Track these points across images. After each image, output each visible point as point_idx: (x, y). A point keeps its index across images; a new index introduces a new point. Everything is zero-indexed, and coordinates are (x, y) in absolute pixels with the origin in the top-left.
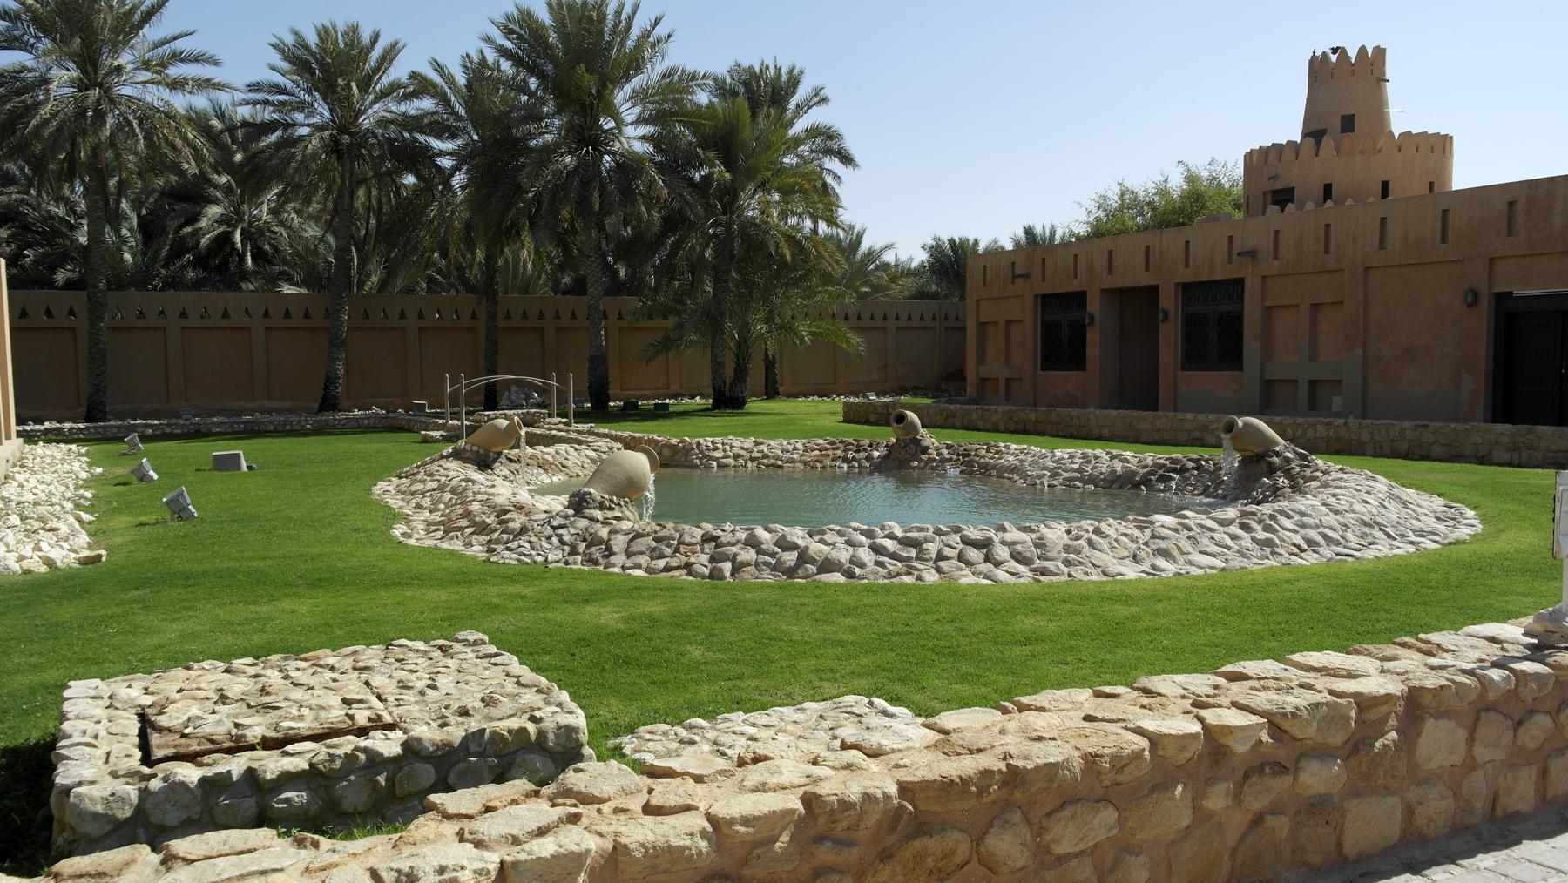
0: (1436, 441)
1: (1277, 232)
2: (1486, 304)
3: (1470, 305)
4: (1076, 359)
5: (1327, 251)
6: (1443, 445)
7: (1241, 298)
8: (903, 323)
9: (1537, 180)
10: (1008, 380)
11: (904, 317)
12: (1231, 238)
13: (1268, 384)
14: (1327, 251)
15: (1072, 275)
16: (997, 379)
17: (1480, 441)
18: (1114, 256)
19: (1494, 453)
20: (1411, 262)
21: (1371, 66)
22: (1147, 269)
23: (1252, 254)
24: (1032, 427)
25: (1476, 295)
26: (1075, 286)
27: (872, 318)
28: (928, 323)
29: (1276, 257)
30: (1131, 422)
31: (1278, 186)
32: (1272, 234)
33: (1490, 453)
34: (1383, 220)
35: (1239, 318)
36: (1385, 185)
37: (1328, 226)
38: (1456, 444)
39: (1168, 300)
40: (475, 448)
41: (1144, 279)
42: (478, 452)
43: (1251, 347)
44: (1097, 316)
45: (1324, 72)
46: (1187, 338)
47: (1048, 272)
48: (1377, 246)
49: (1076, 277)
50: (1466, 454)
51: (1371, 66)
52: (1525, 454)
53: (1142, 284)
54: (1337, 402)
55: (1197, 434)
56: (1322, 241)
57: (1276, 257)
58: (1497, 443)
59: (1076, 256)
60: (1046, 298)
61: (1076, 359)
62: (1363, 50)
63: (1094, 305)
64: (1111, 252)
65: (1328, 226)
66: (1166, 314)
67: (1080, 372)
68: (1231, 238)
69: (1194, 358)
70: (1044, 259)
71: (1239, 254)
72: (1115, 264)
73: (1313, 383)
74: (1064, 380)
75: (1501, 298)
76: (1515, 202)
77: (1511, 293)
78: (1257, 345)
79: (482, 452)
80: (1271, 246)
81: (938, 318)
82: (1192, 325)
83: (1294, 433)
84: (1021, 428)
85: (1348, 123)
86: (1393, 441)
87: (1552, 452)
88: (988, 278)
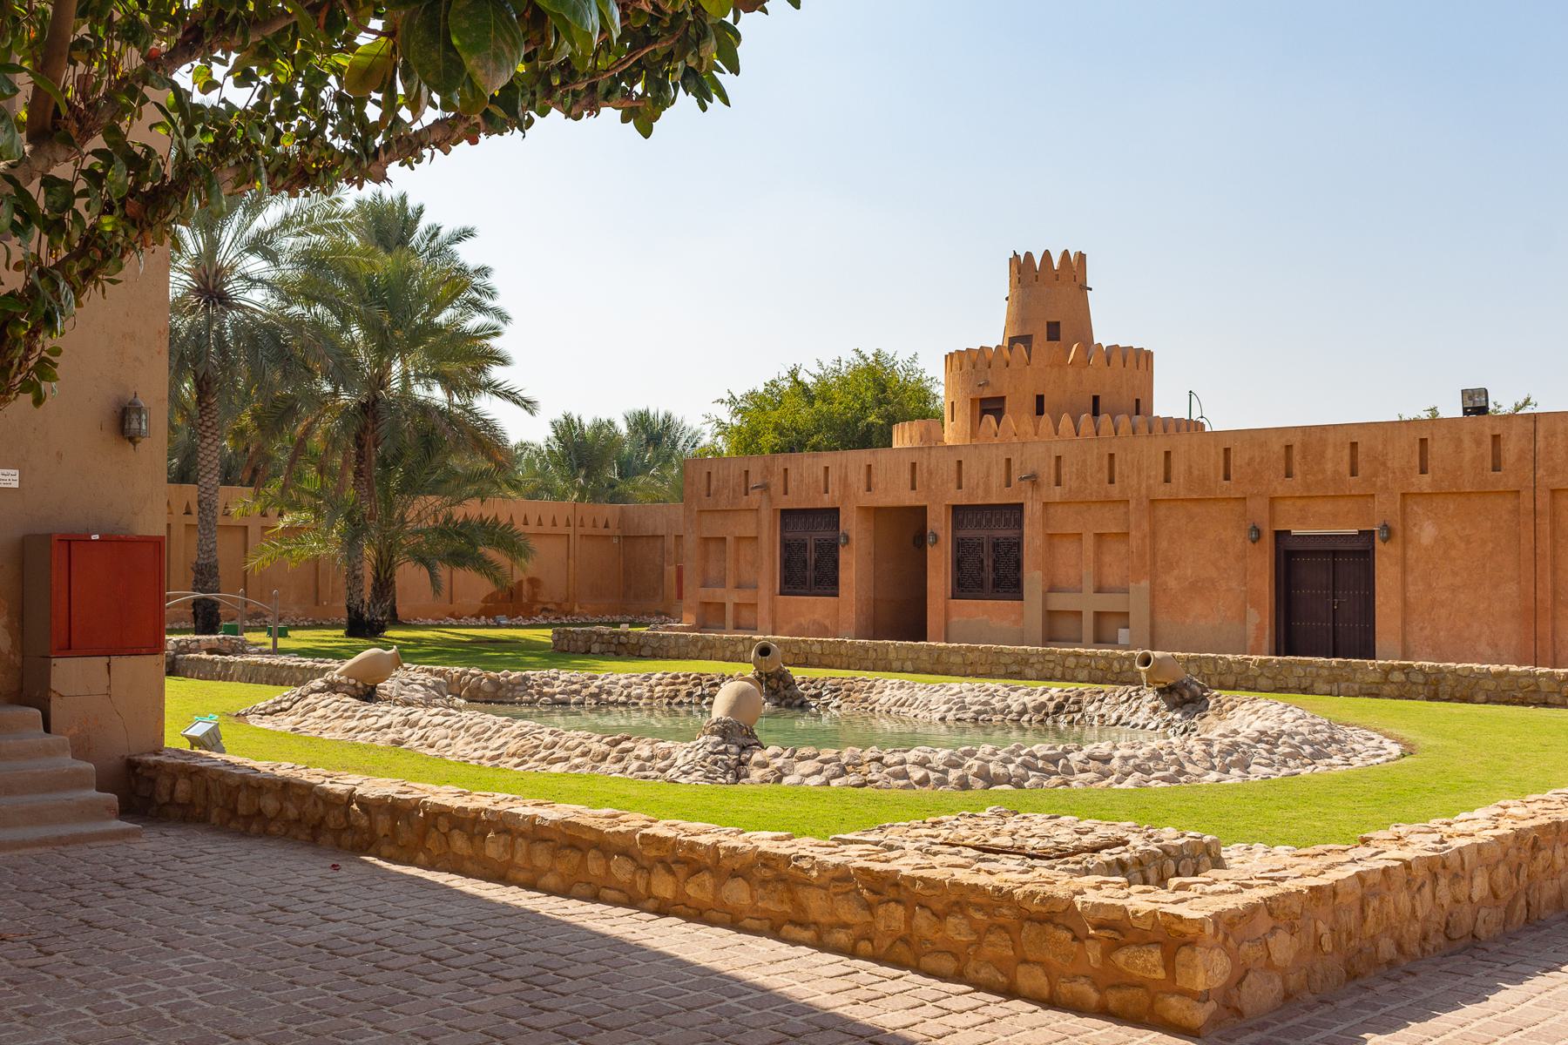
0: (1262, 674)
1: (1058, 458)
2: (1268, 540)
3: (1254, 542)
4: (826, 581)
5: (1111, 481)
6: (1268, 677)
7: (1019, 524)
8: (589, 530)
9: (1324, 428)
10: (1098, 615)
11: (547, 522)
12: (1009, 460)
13: (1050, 615)
14: (1111, 481)
15: (823, 490)
16: (724, 605)
17: (1303, 674)
18: (873, 470)
19: (1316, 685)
20: (1195, 497)
21: (1072, 272)
22: (913, 488)
23: (1033, 479)
24: (817, 661)
25: (1258, 532)
26: (826, 502)
27: (540, 523)
28: (561, 528)
29: (1058, 483)
30: (939, 655)
31: (987, 393)
32: (1053, 462)
33: (1312, 685)
34: (1167, 454)
35: (1017, 545)
36: (1096, 399)
37: (1111, 456)
38: (1280, 677)
39: (939, 523)
40: (352, 681)
41: (909, 499)
42: (355, 685)
43: (1033, 578)
44: (853, 535)
45: (1025, 271)
46: (958, 563)
47: (792, 485)
48: (1162, 479)
49: (826, 492)
50: (1290, 686)
51: (1072, 272)
52: (1343, 686)
53: (907, 503)
54: (1123, 635)
55: (1015, 668)
56: (1106, 471)
57: (1058, 483)
58: (1318, 675)
59: (827, 468)
60: (785, 513)
61: (826, 581)
62: (1047, 255)
63: (851, 524)
64: (870, 466)
65: (1111, 456)
66: (936, 537)
67: (831, 599)
68: (1009, 460)
69: (966, 585)
70: (786, 470)
71: (753, 488)
72: (874, 480)
73: (1098, 615)
74: (813, 607)
75: (1280, 536)
76: (1291, 446)
77: (1290, 531)
78: (1038, 574)
79: (360, 685)
80: (1053, 472)
81: (572, 523)
82: (963, 552)
83: (1121, 668)
84: (802, 660)
85: (1053, 331)
86: (1220, 674)
87: (1367, 684)
88: (712, 488)
